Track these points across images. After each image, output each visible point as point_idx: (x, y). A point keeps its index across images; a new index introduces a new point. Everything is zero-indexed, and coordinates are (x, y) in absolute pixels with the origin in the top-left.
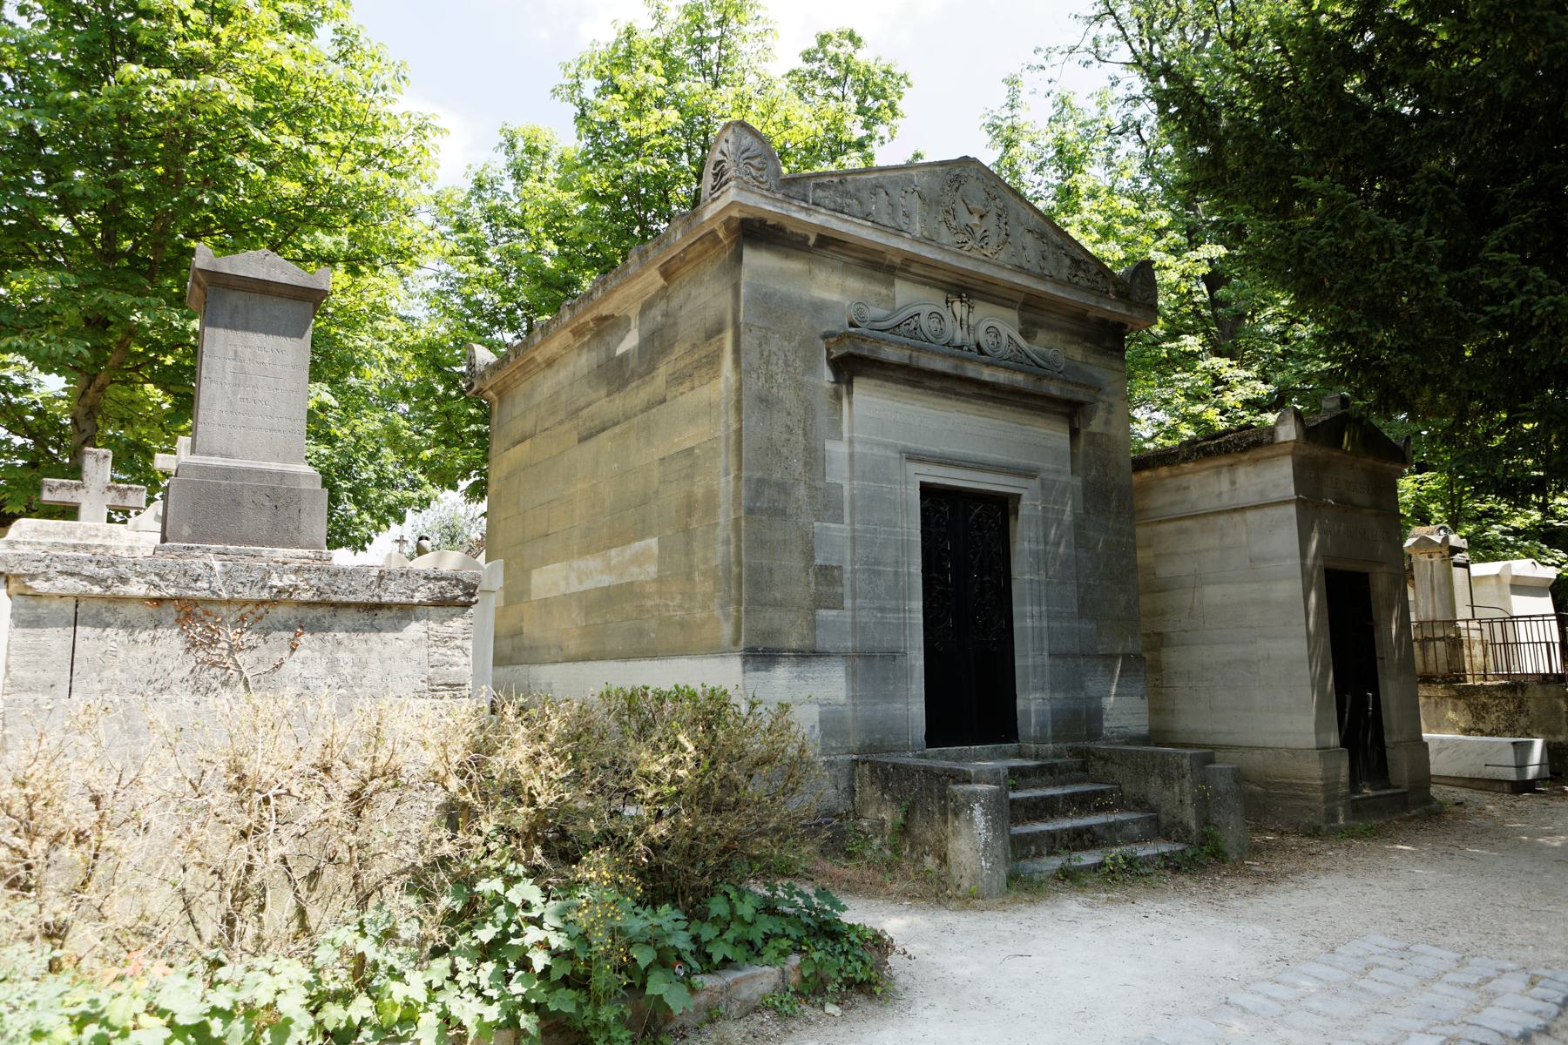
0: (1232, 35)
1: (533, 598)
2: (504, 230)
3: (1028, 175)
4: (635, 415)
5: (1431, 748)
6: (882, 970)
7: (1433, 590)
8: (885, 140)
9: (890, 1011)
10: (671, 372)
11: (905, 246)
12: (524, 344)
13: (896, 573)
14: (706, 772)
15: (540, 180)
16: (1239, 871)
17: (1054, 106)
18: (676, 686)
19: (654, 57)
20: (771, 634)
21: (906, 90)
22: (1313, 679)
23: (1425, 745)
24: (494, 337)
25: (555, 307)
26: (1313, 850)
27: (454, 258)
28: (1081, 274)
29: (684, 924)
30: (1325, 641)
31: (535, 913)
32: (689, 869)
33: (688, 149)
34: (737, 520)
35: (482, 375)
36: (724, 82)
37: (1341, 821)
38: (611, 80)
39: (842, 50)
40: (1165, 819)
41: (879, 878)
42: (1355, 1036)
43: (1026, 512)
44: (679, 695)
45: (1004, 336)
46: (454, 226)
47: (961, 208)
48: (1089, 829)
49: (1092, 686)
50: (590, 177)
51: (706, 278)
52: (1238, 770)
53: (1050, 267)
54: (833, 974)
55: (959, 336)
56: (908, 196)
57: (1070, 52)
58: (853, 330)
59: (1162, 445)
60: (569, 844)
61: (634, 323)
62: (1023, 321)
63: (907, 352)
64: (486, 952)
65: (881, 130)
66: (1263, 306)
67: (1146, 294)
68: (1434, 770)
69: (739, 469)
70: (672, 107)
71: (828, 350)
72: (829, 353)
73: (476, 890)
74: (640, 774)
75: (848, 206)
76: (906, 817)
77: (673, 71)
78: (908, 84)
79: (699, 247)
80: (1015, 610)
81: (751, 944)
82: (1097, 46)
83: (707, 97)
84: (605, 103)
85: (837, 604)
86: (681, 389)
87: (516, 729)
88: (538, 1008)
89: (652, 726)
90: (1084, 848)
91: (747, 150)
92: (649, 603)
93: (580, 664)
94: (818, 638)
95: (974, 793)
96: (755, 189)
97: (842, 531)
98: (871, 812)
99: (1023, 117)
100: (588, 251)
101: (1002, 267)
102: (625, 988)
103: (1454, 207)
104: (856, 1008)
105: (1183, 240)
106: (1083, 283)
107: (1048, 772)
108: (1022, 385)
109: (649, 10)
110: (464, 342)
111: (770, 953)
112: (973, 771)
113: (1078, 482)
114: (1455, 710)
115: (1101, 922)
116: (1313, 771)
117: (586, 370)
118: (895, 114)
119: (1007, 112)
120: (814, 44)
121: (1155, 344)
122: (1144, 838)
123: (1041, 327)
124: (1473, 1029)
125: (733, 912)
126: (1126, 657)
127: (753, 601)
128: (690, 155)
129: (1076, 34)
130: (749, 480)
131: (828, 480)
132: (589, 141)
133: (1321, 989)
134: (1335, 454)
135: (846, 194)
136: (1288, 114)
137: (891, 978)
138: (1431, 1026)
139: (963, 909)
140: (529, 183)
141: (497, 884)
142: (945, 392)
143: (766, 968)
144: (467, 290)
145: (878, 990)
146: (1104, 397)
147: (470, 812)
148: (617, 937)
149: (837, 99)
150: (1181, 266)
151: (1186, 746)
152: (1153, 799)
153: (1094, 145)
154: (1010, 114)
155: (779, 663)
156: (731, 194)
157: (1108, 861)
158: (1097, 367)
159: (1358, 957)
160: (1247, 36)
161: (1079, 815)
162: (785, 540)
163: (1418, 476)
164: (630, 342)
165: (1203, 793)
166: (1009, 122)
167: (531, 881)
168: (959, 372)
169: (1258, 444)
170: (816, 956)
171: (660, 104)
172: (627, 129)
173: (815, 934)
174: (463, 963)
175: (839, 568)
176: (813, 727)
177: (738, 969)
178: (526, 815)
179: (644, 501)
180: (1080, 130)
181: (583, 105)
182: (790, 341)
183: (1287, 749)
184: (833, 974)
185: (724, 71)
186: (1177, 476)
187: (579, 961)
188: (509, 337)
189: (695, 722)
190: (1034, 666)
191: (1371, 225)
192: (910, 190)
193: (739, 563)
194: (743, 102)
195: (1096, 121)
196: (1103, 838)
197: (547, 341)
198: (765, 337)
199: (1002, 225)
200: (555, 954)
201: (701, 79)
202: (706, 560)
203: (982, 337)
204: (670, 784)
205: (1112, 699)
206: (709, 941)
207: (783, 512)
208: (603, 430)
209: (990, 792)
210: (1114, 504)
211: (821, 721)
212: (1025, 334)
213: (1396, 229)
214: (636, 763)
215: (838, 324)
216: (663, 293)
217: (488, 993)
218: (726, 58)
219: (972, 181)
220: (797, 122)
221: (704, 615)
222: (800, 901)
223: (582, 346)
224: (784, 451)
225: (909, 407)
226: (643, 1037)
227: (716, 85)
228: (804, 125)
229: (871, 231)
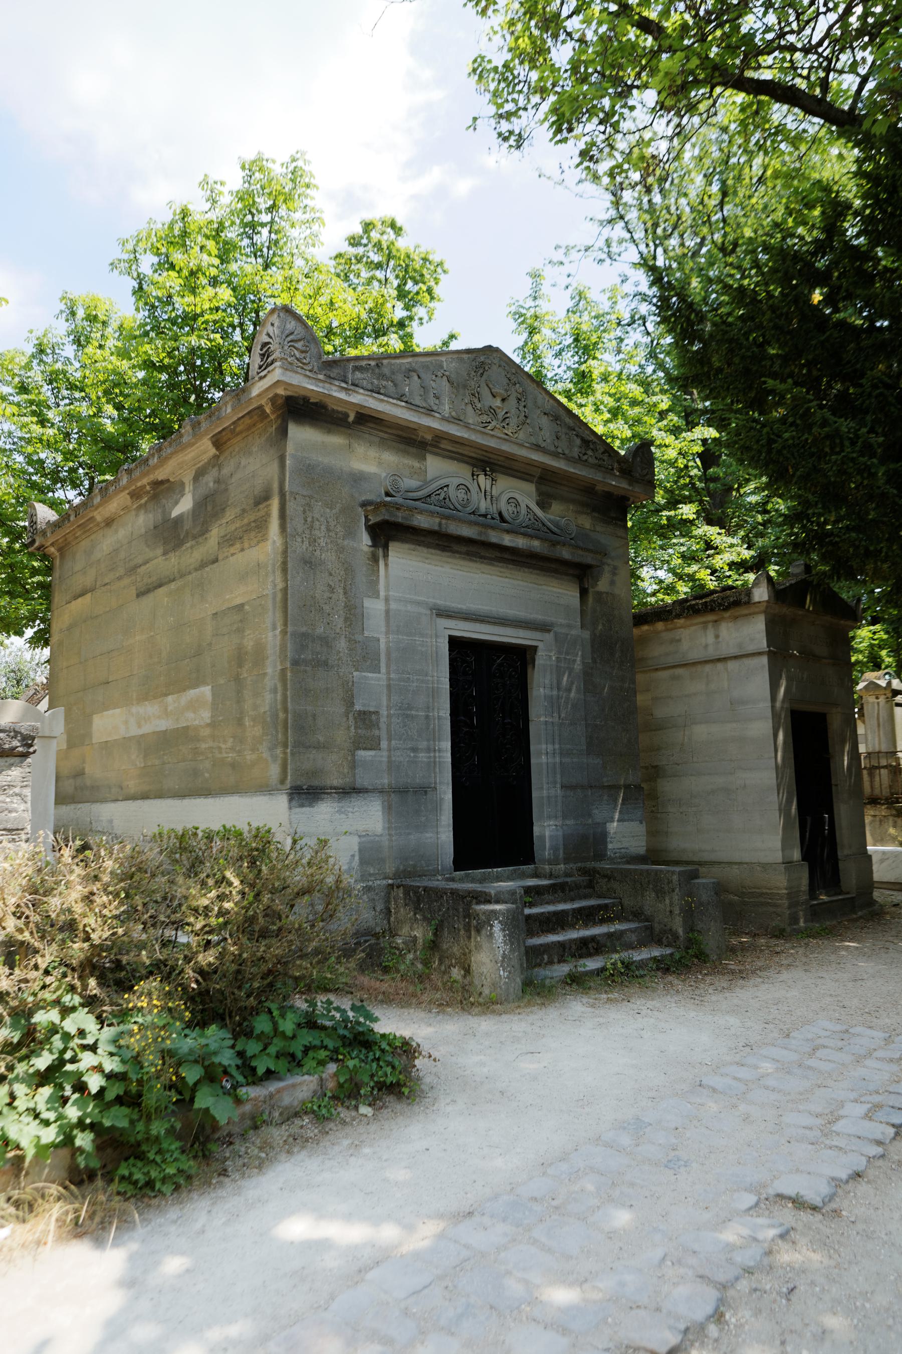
0: (723, 243)
1: (94, 741)
2: (65, 393)
3: (548, 359)
4: (190, 573)
5: (874, 859)
6: (410, 1073)
7: (879, 725)
8: (424, 321)
9: (416, 1108)
10: (222, 534)
11: (435, 424)
12: (83, 504)
13: (427, 717)
14: (251, 904)
15: (101, 347)
16: (718, 969)
17: (572, 298)
18: (224, 826)
19: (207, 237)
20: (315, 773)
21: (442, 277)
22: (780, 805)
23: (869, 858)
24: (56, 495)
25: (115, 468)
26: (778, 949)
27: (15, 418)
28: (590, 453)
29: (231, 1042)
30: (790, 773)
31: (90, 1040)
32: (236, 991)
33: (241, 325)
34: (283, 671)
35: (44, 533)
36: (274, 264)
37: (802, 924)
38: (167, 257)
39: (385, 237)
40: (657, 927)
41: (411, 989)
42: (801, 1107)
43: (541, 662)
44: (226, 834)
45: (523, 506)
46: (16, 387)
47: (485, 392)
48: (593, 938)
49: (598, 814)
50: (147, 347)
51: (255, 449)
52: (718, 884)
53: (563, 446)
54: (366, 1079)
55: (483, 506)
56: (438, 380)
57: (586, 250)
58: (388, 499)
59: (662, 600)
60: (123, 973)
61: (189, 488)
62: (540, 493)
63: (437, 520)
64: (42, 1078)
65: (420, 311)
66: (748, 481)
67: (645, 472)
68: (876, 877)
69: (285, 624)
70: (225, 286)
71: (366, 517)
72: (367, 519)
73: (33, 1021)
74: (190, 908)
75: (384, 387)
76: (435, 934)
77: (226, 253)
78: (444, 272)
79: (247, 421)
80: (533, 748)
81: (293, 1056)
82: (609, 247)
83: (258, 278)
84: (160, 279)
85: (375, 746)
86: (232, 550)
87: (72, 872)
88: (92, 1127)
89: (202, 862)
90: (589, 955)
91: (292, 333)
92: (204, 746)
93: (139, 803)
94: (357, 776)
95: (494, 912)
96: (299, 370)
97: (379, 679)
98: (405, 930)
99: (544, 307)
100: (146, 417)
101: (521, 445)
102: (174, 1103)
103: (893, 409)
104: (387, 1107)
105: (682, 423)
106: (592, 460)
107: (559, 890)
108: (538, 550)
109: (203, 193)
110: (26, 500)
111: (309, 1064)
112: (493, 892)
113: (587, 635)
114: (895, 826)
115: (601, 1020)
116: (779, 882)
117: (143, 531)
118: (432, 298)
119: (530, 303)
120: (358, 230)
121: (658, 511)
122: (642, 944)
123: (555, 499)
124: (893, 1096)
125: (275, 1029)
126: (627, 787)
127: (298, 744)
128: (243, 331)
129: (592, 234)
130: (294, 634)
131: (366, 634)
132: (146, 313)
133: (777, 1068)
134: (800, 613)
135: (382, 376)
136: (761, 323)
137: (419, 1079)
138: (861, 1096)
139: (483, 1013)
140: (90, 350)
141: (54, 1015)
142: (471, 556)
143: (306, 1077)
144: (30, 449)
145: (406, 1091)
146: (609, 561)
147: (28, 950)
148: (167, 1058)
149: (380, 281)
150: (678, 445)
151: (677, 863)
152: (648, 911)
153: (605, 335)
154: (533, 304)
155: (322, 799)
156: (277, 374)
157: (609, 966)
158: (603, 535)
159: (808, 1040)
160: (735, 245)
161: (586, 926)
162: (327, 689)
163: (872, 628)
164: (184, 505)
165: (689, 904)
166: (532, 311)
167: (86, 1010)
168: (483, 538)
169: (737, 604)
170: (351, 1063)
171: (214, 282)
172: (182, 304)
173: (350, 1044)
174: (20, 1089)
175: (377, 713)
176: (353, 856)
177: (280, 1079)
178: (81, 949)
179: (199, 653)
180: (594, 321)
181: (140, 279)
182: (331, 509)
183: (760, 864)
184: (366, 1079)
185: (274, 254)
186: (671, 630)
187: (132, 1082)
188: (71, 494)
189: (241, 858)
190: (549, 797)
191: (825, 423)
192: (439, 374)
193: (286, 710)
194: (291, 285)
195: (607, 314)
196: (605, 946)
197: (106, 502)
198: (309, 505)
199: (521, 408)
200: (110, 1076)
201: (254, 261)
202: (255, 707)
203: (503, 506)
204: (217, 917)
205: (615, 824)
206: (254, 1056)
207: (326, 664)
208: (160, 586)
209: (508, 910)
210: (618, 655)
211: (360, 851)
212: (542, 505)
213: (845, 425)
214: (186, 898)
215: (374, 493)
216: (215, 462)
217: (45, 1115)
218: (276, 242)
219: (495, 368)
220: (341, 304)
221: (254, 757)
222: (338, 1015)
223: (140, 507)
224: (327, 608)
225: (439, 568)
226: (192, 1146)
227: (266, 266)
228: (347, 307)
229: (405, 411)
